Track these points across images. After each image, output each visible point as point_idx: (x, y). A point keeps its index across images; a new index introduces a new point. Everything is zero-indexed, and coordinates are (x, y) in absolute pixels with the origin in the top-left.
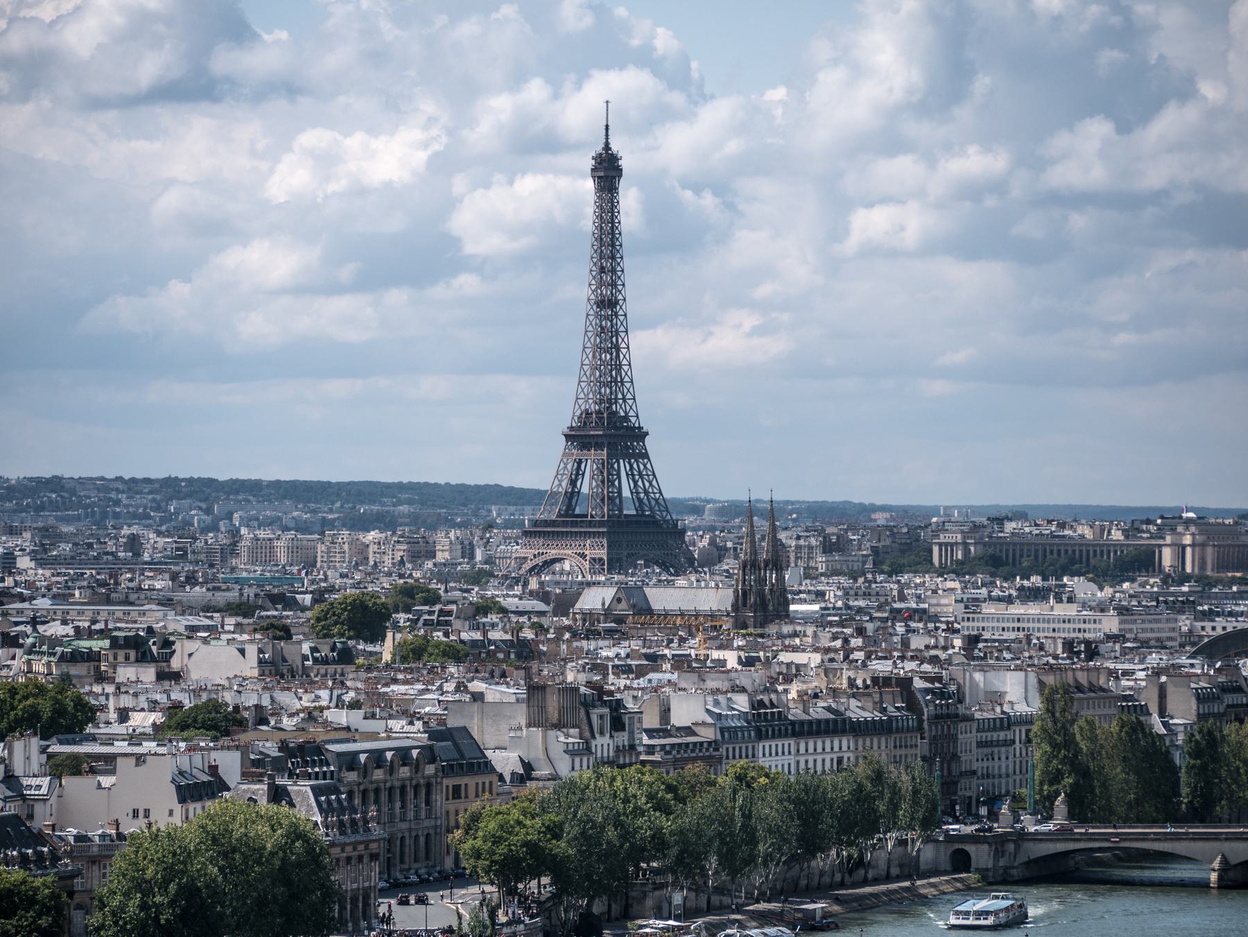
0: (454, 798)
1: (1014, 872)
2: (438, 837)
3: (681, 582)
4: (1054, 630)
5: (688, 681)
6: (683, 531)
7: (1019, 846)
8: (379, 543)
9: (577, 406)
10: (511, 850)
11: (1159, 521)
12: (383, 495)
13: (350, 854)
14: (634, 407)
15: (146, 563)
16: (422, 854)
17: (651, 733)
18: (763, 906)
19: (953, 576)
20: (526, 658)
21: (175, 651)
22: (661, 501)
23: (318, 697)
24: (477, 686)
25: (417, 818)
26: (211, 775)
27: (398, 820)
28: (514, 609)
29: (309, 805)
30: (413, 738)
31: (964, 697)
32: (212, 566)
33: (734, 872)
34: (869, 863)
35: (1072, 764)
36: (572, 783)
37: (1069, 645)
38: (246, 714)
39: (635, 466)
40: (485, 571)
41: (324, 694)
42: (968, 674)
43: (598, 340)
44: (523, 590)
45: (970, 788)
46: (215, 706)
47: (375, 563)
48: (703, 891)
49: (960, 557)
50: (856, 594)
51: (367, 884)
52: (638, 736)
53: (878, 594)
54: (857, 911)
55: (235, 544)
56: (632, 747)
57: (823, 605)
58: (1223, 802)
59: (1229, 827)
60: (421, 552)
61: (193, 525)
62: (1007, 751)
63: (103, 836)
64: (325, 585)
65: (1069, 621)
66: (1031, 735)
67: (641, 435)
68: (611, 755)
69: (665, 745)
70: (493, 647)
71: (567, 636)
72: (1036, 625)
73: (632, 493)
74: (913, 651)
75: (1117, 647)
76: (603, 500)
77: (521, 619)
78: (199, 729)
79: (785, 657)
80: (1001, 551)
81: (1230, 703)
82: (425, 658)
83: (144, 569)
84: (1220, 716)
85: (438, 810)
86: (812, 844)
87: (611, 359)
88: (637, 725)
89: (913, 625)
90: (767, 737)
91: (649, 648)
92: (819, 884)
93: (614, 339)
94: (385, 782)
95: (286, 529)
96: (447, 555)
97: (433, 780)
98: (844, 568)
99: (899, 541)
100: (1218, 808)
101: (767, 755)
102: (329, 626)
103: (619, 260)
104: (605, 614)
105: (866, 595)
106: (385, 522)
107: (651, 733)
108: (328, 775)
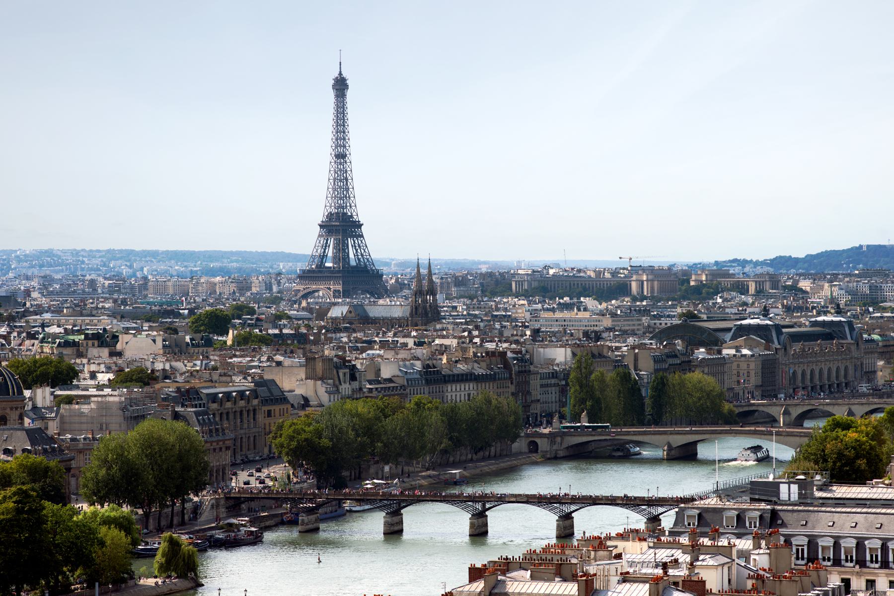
0: (268, 417)
5: (389, 355)
9: (326, 210)
16: (252, 446)
17: (370, 382)
18: (429, 473)
19: (523, 298)
22: (370, 260)
23: (195, 365)
24: (279, 358)
27: (239, 429)
39: (356, 241)
43: (336, 175)
46: (142, 371)
48: (399, 464)
49: (526, 288)
50: (474, 308)
51: (224, 463)
56: (361, 389)
65: (557, 321)
76: (339, 259)
77: (299, 322)
93: (345, 175)
97: (257, 407)
105: (479, 308)
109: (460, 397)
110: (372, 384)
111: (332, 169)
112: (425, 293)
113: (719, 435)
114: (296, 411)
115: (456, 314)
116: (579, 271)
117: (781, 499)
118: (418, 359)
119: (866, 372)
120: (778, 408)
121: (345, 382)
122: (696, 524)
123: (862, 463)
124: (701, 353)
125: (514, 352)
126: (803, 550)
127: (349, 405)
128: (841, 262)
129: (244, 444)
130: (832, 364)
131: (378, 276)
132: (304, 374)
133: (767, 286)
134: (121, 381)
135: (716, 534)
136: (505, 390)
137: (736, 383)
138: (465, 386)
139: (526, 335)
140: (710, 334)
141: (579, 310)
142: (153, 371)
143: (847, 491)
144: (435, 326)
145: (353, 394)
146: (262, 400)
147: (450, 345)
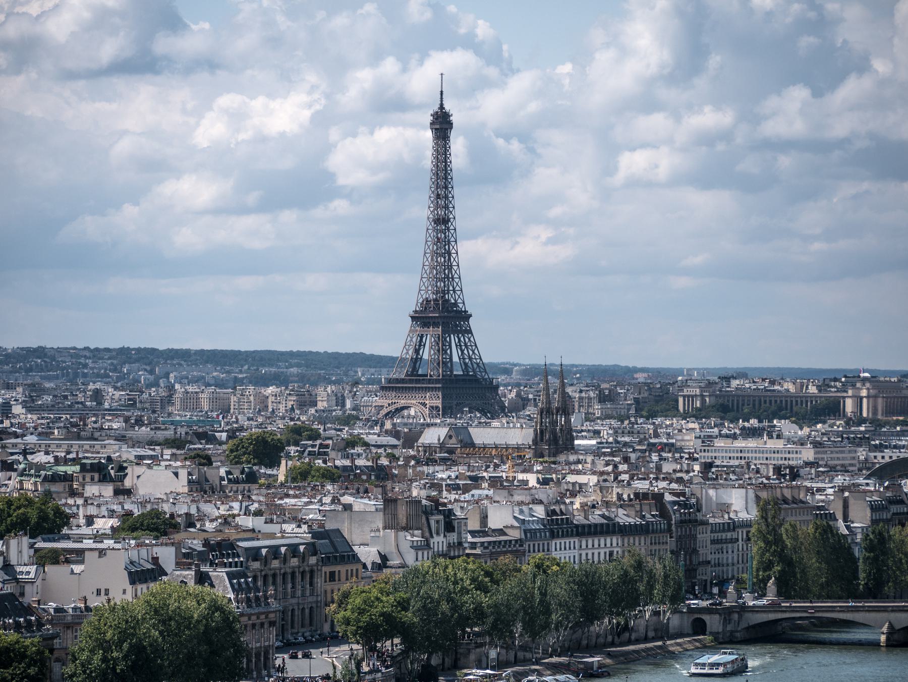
0: (330, 581)
1: (738, 635)
2: (319, 609)
3: (495, 423)
4: (767, 459)
5: (500, 496)
6: (497, 387)
7: (741, 616)
8: (276, 395)
9: (420, 296)
10: (372, 619)
11: (843, 379)
12: (278, 360)
13: (255, 622)
14: (461, 296)
15: (106, 410)
16: (307, 621)
17: (473, 533)
18: (555, 659)
19: (693, 419)
20: (382, 479)
21: (127, 474)
22: (481, 365)
23: (231, 507)
24: (347, 499)
25: (303, 595)
26: (154, 564)
27: (289, 597)
28: (374, 443)
29: (225, 586)
30: (300, 538)
31: (701, 507)
32: (154, 412)
33: (534, 635)
34: (632, 628)
35: (780, 556)
36: (416, 570)
37: (778, 470)
38: (179, 520)
39: (462, 339)
40: (353, 416)
41: (236, 505)
42: (704, 490)
43: (435, 247)
44: (381, 429)
45: (706, 574)
46: (157, 514)
47: (273, 410)
48: (511, 649)
49: (698, 405)
50: (623, 433)
51: (267, 644)
52: (465, 536)
53: (638, 432)
54: (623, 663)
55: (171, 396)
56: (460, 544)
57: (599, 440)
58: (890, 584)
59: (894, 602)
60: (306, 402)
61: (140, 382)
62: (733, 547)
63: (75, 609)
64: (236, 426)
65: (778, 452)
66: (750, 535)
67: (466, 317)
68: (445, 549)
69: (484, 542)
70: (358, 471)
71: (413, 463)
72: (754, 455)
73: (460, 359)
74: (664, 474)
75: (813, 471)
76: (438, 364)
77: (379, 451)
78: (145, 530)
79: (571, 478)
80: (728, 401)
81: (895, 511)
82: (310, 479)
83: (105, 414)
84: (887, 521)
85: (319, 590)
86: (591, 614)
87: (445, 261)
88: (463, 528)
89: (664, 455)
90: (558, 537)
91: (472, 471)
92: (596, 643)
93: (447, 247)
94: (280, 569)
95: (208, 385)
96: (325, 404)
97: (315, 568)
98: (614, 413)
99: (654, 394)
100: (886, 588)
101: (558, 549)
102: (239, 456)
103: (450, 189)
104: (440, 447)
105: (630, 433)
106: (280, 380)
107: (473, 533)
108: (239, 564)
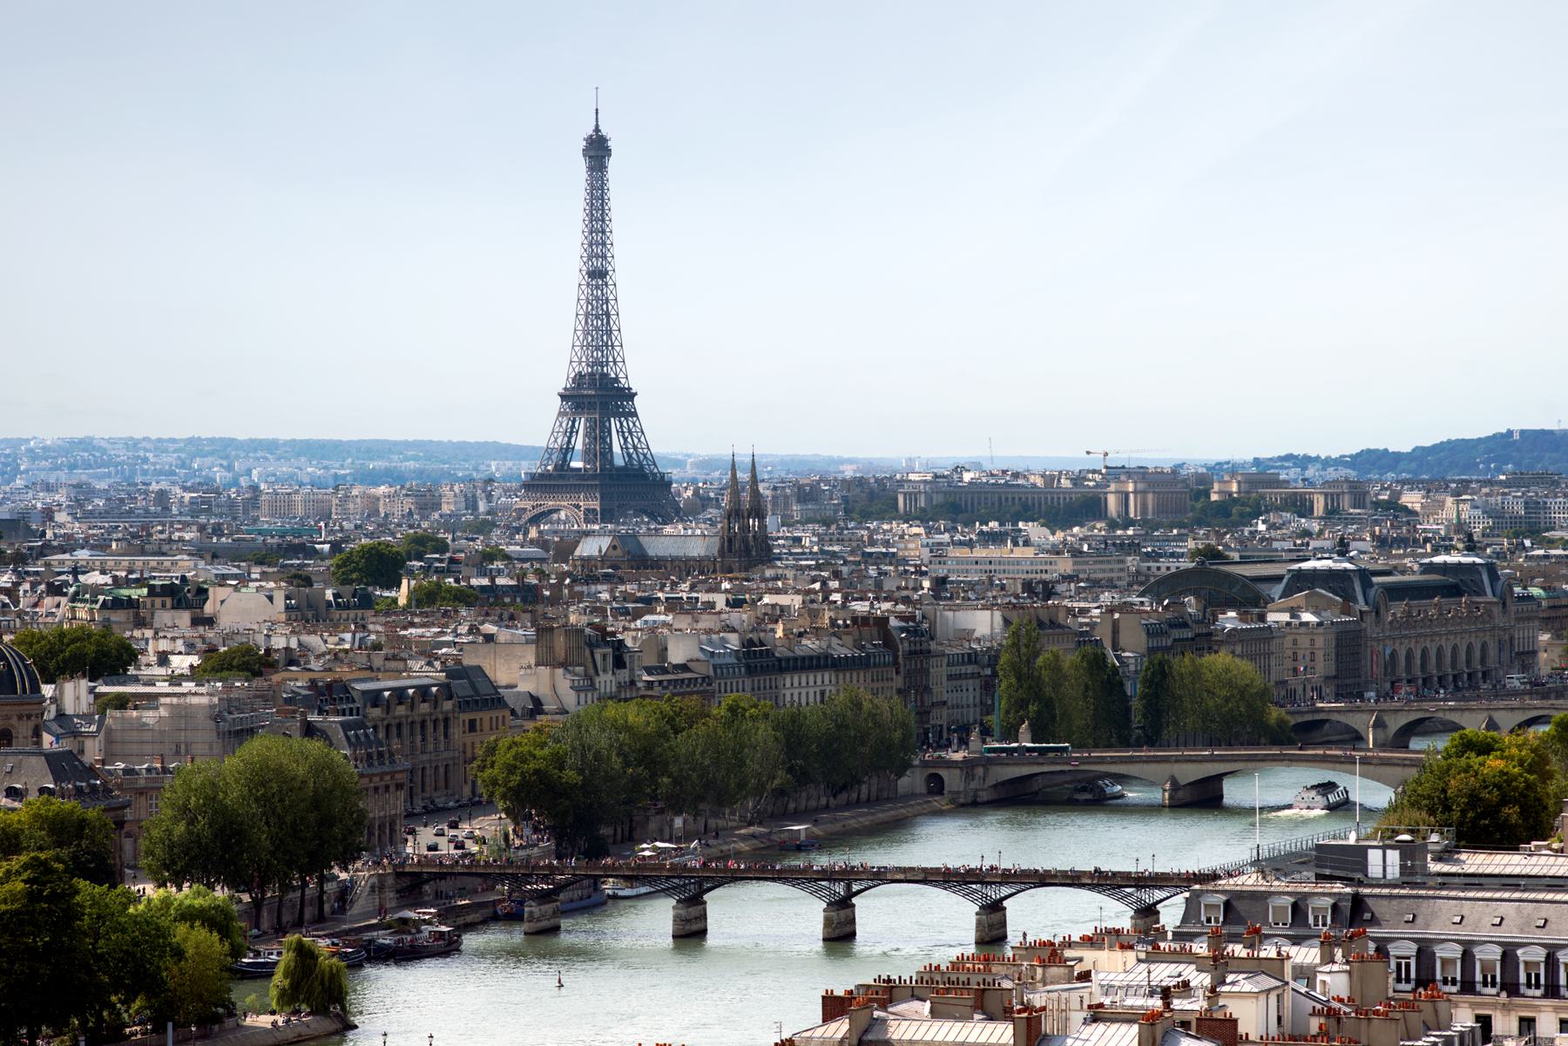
0: (470, 731)
5: (683, 622)
9: (571, 369)
16: (442, 783)
17: (649, 671)
18: (752, 829)
19: (918, 522)
22: (649, 456)
23: (342, 640)
24: (489, 628)
27: (419, 752)
39: (625, 424)
43: (590, 307)
46: (249, 651)
48: (700, 815)
49: (923, 505)
50: (831, 540)
51: (393, 812)
56: (633, 683)
65: (977, 563)
77: (525, 566)
93: (605, 307)
97: (451, 715)
105: (840, 541)
109: (807, 697)
110: (653, 674)
111: (583, 297)
112: (746, 514)
113: (1261, 764)
114: (519, 722)
115: (800, 550)
116: (1016, 475)
117: (1370, 875)
118: (734, 630)
119: (1519, 654)
120: (1365, 716)
121: (605, 671)
122: (1221, 919)
123: (1512, 813)
124: (1229, 619)
125: (901, 617)
126: (1408, 966)
127: (612, 711)
128: (1475, 459)
129: (427, 780)
130: (1458, 639)
131: (664, 484)
132: (534, 657)
133: (1346, 501)
134: (213, 669)
135: (1255, 938)
136: (886, 684)
137: (1291, 673)
138: (815, 677)
139: (923, 589)
140: (1244, 586)
141: (1016, 544)
142: (268, 651)
143: (1485, 862)
144: (763, 572)
145: (619, 692)
146: (459, 702)
147: (789, 606)
